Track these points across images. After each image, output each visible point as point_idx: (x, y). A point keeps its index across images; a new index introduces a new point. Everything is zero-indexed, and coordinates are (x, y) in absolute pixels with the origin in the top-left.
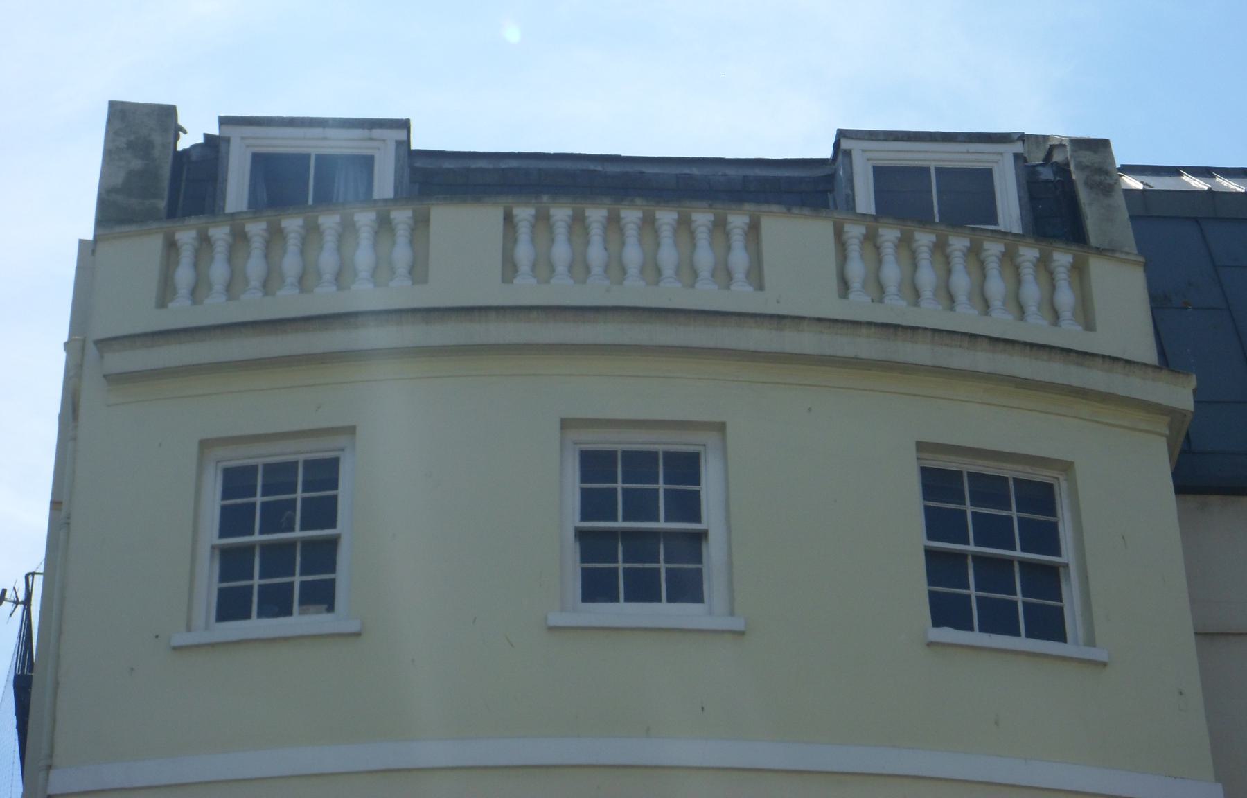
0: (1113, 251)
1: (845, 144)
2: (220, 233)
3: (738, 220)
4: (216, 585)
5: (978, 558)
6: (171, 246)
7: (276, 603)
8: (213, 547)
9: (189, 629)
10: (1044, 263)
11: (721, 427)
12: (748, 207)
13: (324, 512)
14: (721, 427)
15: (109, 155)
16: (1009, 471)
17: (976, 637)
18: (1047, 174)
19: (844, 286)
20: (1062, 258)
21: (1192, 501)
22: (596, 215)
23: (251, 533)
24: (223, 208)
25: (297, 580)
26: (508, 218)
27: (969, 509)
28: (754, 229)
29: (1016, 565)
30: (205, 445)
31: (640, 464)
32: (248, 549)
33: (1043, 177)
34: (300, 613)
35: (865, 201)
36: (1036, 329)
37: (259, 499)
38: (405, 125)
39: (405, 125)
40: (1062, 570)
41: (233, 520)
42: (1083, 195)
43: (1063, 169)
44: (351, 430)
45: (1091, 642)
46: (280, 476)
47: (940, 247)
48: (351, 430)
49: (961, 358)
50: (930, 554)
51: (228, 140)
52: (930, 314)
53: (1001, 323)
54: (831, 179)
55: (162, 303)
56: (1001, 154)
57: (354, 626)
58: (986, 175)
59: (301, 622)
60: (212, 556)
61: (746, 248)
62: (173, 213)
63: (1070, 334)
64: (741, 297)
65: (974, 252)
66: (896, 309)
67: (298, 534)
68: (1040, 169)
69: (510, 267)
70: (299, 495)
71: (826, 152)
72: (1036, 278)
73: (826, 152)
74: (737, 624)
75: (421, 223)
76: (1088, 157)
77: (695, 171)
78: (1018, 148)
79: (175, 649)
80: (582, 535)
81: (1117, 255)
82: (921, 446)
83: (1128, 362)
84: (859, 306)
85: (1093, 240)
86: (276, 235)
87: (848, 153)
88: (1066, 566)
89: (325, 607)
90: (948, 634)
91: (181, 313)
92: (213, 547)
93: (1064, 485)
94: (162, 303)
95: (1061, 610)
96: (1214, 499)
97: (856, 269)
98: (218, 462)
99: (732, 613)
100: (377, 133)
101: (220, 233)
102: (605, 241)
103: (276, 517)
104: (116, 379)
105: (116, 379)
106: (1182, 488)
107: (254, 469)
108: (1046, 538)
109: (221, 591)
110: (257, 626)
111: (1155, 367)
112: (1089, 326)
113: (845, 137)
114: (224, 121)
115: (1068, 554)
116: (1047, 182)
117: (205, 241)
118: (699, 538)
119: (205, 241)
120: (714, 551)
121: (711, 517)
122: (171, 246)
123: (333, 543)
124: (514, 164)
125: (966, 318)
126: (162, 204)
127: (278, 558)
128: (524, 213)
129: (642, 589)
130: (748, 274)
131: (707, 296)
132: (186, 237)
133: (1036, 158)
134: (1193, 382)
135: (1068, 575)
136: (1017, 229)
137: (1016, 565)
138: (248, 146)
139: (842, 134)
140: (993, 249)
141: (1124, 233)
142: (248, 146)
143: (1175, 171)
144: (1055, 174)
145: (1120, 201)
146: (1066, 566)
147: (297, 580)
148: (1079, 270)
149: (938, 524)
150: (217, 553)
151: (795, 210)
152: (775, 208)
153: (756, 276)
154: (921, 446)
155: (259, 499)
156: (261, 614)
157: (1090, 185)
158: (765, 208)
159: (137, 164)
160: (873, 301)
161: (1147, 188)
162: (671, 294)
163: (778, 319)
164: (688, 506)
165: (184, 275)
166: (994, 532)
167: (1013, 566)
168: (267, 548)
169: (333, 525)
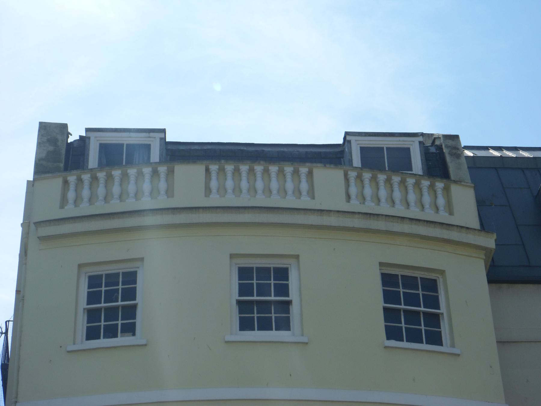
0: (461, 182)
1: (348, 138)
2: (86, 177)
3: (304, 170)
4: (85, 325)
5: (405, 311)
6: (66, 182)
7: (111, 333)
8: (84, 309)
9: (74, 344)
10: (432, 187)
11: (297, 257)
12: (308, 164)
13: (130, 294)
14: (297, 257)
15: (40, 144)
16: (418, 274)
17: (405, 344)
18: (433, 150)
19: (348, 197)
20: (440, 185)
21: (495, 286)
22: (244, 168)
23: (100, 303)
24: (88, 167)
25: (120, 322)
26: (207, 170)
27: (401, 290)
28: (310, 174)
29: (422, 314)
30: (80, 266)
31: (264, 272)
32: (99, 310)
33: (431, 151)
34: (121, 336)
35: (357, 161)
36: (429, 215)
37: (103, 289)
38: (163, 131)
39: (163, 131)
40: (440, 315)
41: (92, 298)
42: (448, 158)
43: (440, 148)
44: (142, 259)
45: (453, 346)
46: (112, 279)
47: (388, 181)
48: (142, 259)
49: (381, 225)
50: (385, 309)
51: (89, 138)
52: (385, 209)
53: (414, 212)
54: (342, 152)
55: (62, 206)
56: (414, 141)
57: (144, 342)
58: (407, 151)
59: (121, 340)
60: (84, 312)
61: (307, 181)
62: (67, 168)
63: (443, 217)
64: (305, 202)
65: (403, 182)
66: (370, 207)
67: (120, 303)
68: (429, 147)
69: (208, 190)
70: (120, 287)
71: (341, 142)
72: (414, 191)
73: (341, 142)
74: (305, 340)
75: (171, 172)
76: (450, 143)
77: (285, 150)
78: (421, 139)
79: (68, 352)
80: (239, 302)
81: (463, 183)
82: (381, 264)
83: (467, 228)
84: (355, 206)
85: (453, 177)
86: (109, 178)
87: (349, 142)
88: (442, 314)
89: (132, 333)
90: (393, 343)
91: (70, 211)
92: (84, 309)
93: (441, 280)
94: (62, 206)
95: (440, 332)
96: (504, 286)
97: (353, 190)
98: (86, 273)
99: (302, 335)
100: (152, 134)
101: (86, 177)
102: (218, 179)
103: (111, 296)
104: (42, 239)
105: (42, 239)
106: (491, 280)
107: (118, 274)
108: (434, 302)
109: (88, 327)
110: (103, 342)
111: (479, 230)
112: (451, 213)
113: (348, 135)
114: (88, 130)
115: (443, 309)
116: (433, 153)
117: (80, 180)
118: (288, 303)
119: (80, 180)
120: (295, 309)
121: (293, 295)
122: (66, 182)
123: (135, 307)
124: (210, 147)
125: (399, 210)
126: (62, 165)
127: (111, 313)
128: (214, 168)
129: (265, 325)
130: (308, 193)
131: (290, 202)
132: (72, 179)
133: (428, 143)
134: (495, 236)
135: (443, 317)
136: (420, 173)
137: (422, 314)
138: (98, 140)
139: (347, 134)
140: (411, 181)
141: (465, 174)
142: (98, 140)
143: (486, 148)
144: (436, 150)
145: (463, 161)
146: (442, 314)
147: (120, 322)
148: (447, 189)
149: (389, 297)
150: (86, 311)
151: (328, 166)
152: (319, 165)
153: (312, 193)
154: (381, 264)
155: (103, 289)
156: (104, 338)
157: (451, 154)
158: (315, 165)
159: (51, 148)
160: (360, 203)
161: (475, 155)
162: (276, 201)
163: (321, 212)
164: (283, 290)
165: (71, 195)
166: (412, 300)
167: (420, 314)
168: (107, 309)
169: (135, 300)
